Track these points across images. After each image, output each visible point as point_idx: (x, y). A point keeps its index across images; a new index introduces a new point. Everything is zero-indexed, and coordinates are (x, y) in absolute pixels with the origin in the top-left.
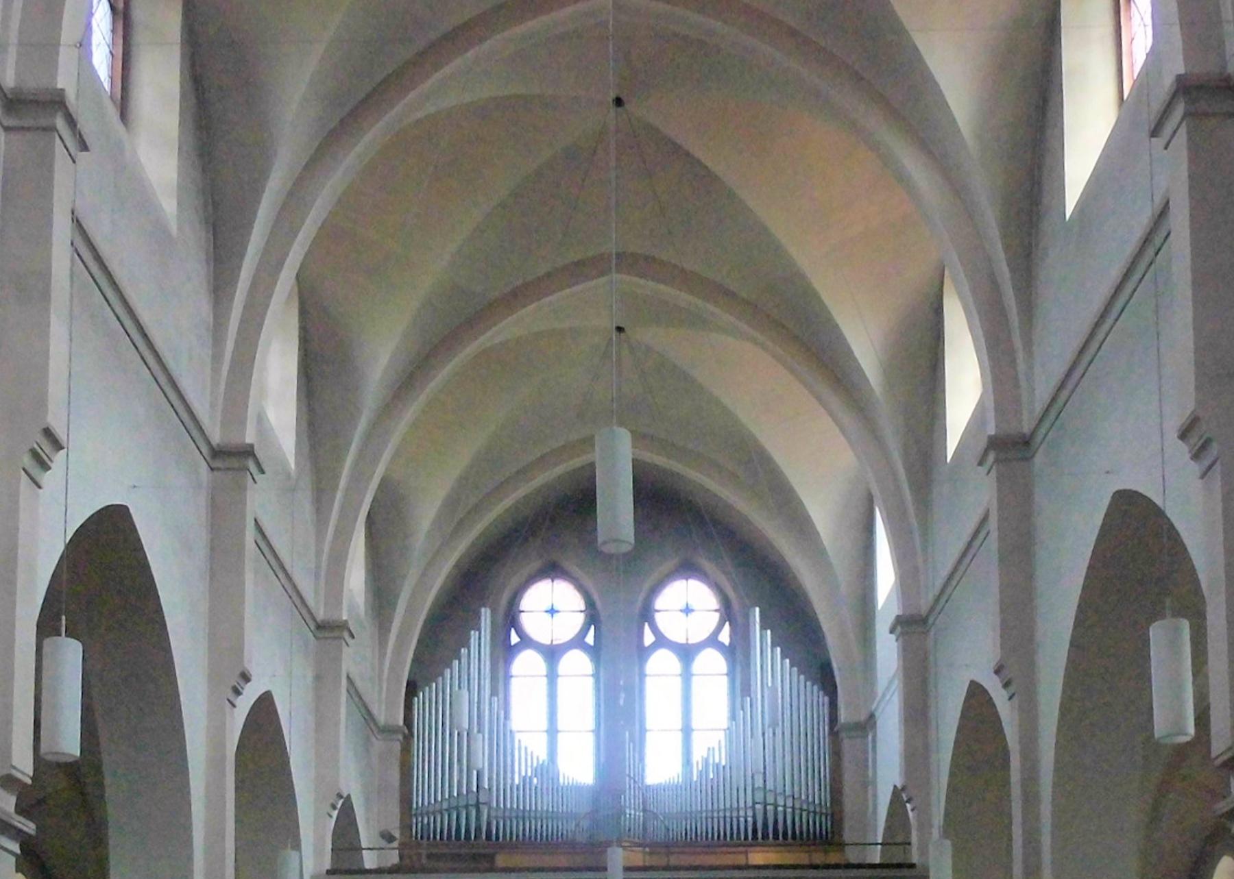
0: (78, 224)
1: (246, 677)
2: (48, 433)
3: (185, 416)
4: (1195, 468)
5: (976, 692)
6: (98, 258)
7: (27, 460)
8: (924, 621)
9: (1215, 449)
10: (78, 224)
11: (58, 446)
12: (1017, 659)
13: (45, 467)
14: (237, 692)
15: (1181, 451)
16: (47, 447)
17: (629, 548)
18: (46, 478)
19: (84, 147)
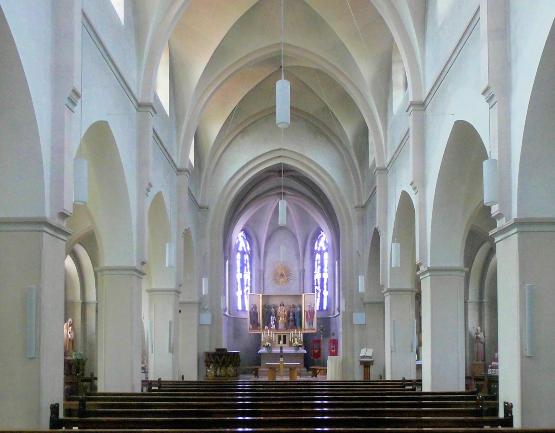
0: (84, 15)
1: (150, 185)
2: (74, 91)
3: (102, 50)
4: (487, 105)
5: (405, 196)
6: (122, 78)
7: (67, 101)
8: (385, 169)
9: (495, 99)
10: (84, 15)
11: (79, 96)
12: (420, 182)
13: (74, 104)
14: (148, 190)
15: (483, 99)
16: (74, 97)
17: (287, 126)
18: (77, 109)
19: (156, 113)
